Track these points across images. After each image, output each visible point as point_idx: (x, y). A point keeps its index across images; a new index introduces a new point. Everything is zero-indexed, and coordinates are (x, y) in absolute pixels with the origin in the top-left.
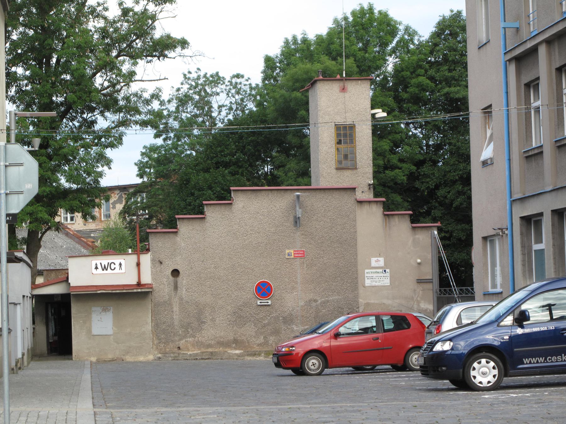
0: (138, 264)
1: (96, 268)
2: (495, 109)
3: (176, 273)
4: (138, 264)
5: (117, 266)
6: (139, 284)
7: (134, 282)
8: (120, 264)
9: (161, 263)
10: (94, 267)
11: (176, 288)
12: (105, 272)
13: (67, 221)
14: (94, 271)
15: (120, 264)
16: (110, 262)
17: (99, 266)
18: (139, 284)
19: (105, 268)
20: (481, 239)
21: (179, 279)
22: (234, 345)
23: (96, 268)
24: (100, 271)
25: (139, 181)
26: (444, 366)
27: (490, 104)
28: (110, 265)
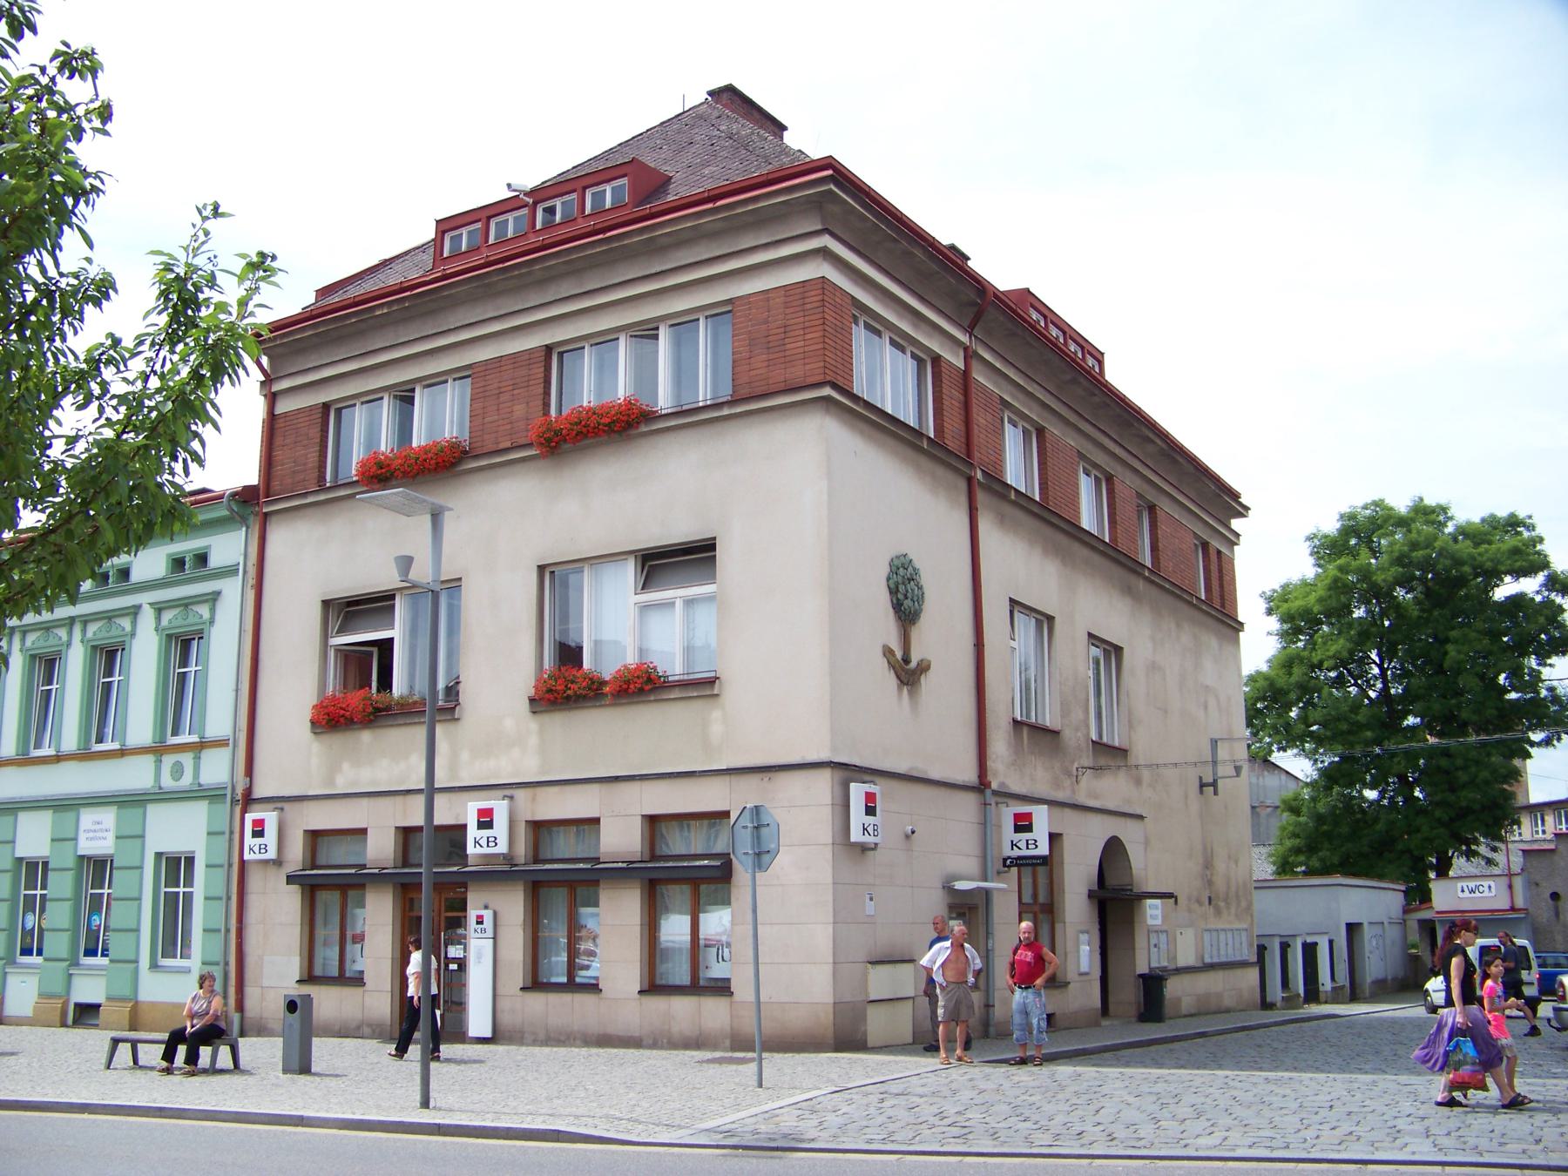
0: (1510, 887)
1: (1463, 891)
2: (97, 820)
3: (1555, 896)
4: (1510, 887)
5: (1486, 889)
6: (1513, 909)
7: (1506, 906)
8: (1490, 887)
9: (1537, 884)
10: (1460, 889)
11: (1557, 914)
12: (1473, 895)
13: (870, 797)
14: (1461, 895)
15: (1490, 887)
16: (1478, 883)
17: (1466, 889)
18: (1513, 909)
19: (1472, 891)
20: (316, 612)
21: (1561, 903)
22: (895, 601)
23: (1463, 891)
24: (1467, 894)
25: (701, 936)
26: (11, 325)
27: (364, 826)
28: (1477, 887)
